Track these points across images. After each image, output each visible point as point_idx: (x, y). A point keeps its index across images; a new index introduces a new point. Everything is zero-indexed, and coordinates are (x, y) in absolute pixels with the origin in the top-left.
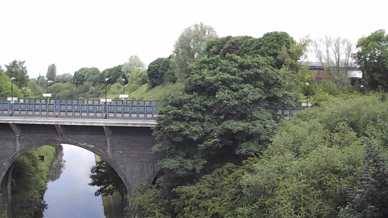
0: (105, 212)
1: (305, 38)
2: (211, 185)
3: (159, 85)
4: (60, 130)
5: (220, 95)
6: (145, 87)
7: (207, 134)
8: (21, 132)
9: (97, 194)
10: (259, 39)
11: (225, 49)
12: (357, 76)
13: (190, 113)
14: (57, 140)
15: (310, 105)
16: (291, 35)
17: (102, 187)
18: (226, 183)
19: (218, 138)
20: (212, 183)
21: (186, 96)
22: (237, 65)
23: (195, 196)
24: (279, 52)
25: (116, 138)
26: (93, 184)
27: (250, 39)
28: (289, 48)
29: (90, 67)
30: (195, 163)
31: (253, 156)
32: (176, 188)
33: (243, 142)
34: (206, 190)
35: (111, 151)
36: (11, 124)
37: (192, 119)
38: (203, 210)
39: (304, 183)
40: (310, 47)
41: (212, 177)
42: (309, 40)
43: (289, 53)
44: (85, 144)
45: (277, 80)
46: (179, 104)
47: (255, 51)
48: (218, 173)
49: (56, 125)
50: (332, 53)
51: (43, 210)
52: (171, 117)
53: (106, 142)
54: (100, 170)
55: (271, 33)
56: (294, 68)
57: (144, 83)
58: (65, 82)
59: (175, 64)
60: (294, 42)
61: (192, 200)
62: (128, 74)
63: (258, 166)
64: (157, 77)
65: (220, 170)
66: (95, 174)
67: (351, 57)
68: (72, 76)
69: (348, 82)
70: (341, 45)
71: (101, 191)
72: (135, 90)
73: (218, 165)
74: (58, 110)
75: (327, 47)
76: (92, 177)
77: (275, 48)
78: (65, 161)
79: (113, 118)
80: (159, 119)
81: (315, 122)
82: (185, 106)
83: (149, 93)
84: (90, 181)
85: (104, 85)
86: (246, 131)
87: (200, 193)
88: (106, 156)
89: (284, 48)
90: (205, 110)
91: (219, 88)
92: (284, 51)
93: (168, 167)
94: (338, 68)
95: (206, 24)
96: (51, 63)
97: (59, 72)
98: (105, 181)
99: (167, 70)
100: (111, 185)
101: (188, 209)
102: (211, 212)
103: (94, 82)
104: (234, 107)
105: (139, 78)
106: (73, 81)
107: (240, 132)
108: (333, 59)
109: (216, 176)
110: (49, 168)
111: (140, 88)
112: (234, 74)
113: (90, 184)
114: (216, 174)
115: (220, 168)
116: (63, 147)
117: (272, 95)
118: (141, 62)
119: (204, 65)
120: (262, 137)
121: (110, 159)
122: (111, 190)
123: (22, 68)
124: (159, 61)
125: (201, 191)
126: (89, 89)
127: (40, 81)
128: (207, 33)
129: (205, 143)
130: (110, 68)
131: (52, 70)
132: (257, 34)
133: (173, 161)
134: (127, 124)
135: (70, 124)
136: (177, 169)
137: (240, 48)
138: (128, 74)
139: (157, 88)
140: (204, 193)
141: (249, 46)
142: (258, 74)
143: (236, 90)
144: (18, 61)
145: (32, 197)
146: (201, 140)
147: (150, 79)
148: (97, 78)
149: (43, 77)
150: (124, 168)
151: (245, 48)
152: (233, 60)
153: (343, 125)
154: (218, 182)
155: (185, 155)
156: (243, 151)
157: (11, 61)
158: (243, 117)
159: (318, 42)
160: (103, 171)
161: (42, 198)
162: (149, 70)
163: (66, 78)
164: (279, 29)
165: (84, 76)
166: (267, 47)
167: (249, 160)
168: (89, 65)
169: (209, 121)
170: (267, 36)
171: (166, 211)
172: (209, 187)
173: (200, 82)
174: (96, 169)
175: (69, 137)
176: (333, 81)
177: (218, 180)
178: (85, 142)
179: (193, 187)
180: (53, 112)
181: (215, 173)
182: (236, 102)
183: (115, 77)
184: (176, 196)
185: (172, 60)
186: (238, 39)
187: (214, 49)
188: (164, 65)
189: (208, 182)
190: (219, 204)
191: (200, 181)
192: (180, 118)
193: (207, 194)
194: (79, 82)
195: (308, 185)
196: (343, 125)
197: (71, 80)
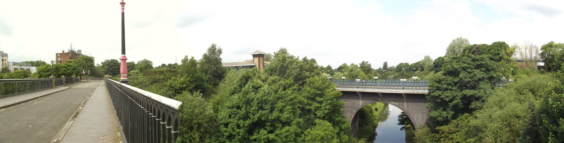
1: (514, 45)
4: (380, 96)
5: (461, 76)
6: (433, 72)
7: (454, 97)
9: (402, 129)
10: (490, 46)
11: (473, 51)
12: (541, 65)
15: (513, 80)
16: (507, 44)
17: (404, 125)
18: (463, 124)
19: (460, 99)
20: (456, 125)
21: (443, 77)
23: (446, 132)
24: (501, 52)
26: (400, 124)
28: (506, 50)
29: (404, 62)
31: (478, 109)
33: (473, 101)
34: (453, 128)
37: (446, 89)
38: (451, 140)
39: (501, 124)
40: (517, 50)
41: (457, 121)
42: (516, 46)
43: (506, 53)
45: (493, 67)
46: (439, 82)
47: (488, 52)
48: (460, 119)
50: (528, 53)
52: (435, 88)
54: (403, 117)
55: (497, 42)
56: (508, 61)
57: (432, 70)
58: (392, 71)
60: (508, 47)
62: (424, 66)
63: (478, 115)
65: (461, 117)
66: (401, 118)
67: (538, 55)
69: (536, 68)
70: (533, 49)
71: (403, 128)
72: (427, 74)
73: (460, 115)
74: (379, 85)
75: (526, 50)
76: (399, 120)
77: (499, 50)
79: (407, 89)
80: (429, 90)
81: (512, 90)
82: (442, 82)
84: (398, 122)
85: (411, 72)
87: (449, 130)
89: (503, 50)
91: (461, 72)
92: (503, 52)
93: (433, 115)
94: (531, 61)
95: (463, 38)
96: (385, 61)
97: (389, 66)
100: (409, 125)
102: (455, 141)
104: (469, 82)
105: (429, 68)
107: (470, 96)
108: (529, 56)
109: (459, 120)
110: (380, 114)
111: (430, 73)
112: (469, 64)
113: (398, 124)
114: (459, 119)
115: (461, 116)
117: (491, 75)
119: (453, 60)
120: (484, 99)
121: (406, 111)
122: (409, 128)
124: (439, 58)
125: (450, 129)
127: (379, 71)
128: (464, 43)
129: (453, 102)
130: (414, 63)
131: (385, 65)
132: (490, 43)
134: (385, 91)
135: (391, 92)
137: (480, 50)
138: (424, 66)
140: (451, 131)
142: (482, 64)
143: (470, 73)
144: (365, 61)
146: (451, 101)
148: (408, 68)
149: (381, 68)
153: (526, 91)
154: (460, 124)
155: (442, 109)
157: (362, 61)
158: (474, 88)
159: (521, 47)
161: (374, 130)
162: (434, 63)
163: (392, 69)
164: (501, 40)
166: (494, 50)
169: (455, 90)
170: (494, 44)
171: (433, 140)
172: (455, 127)
173: (450, 69)
174: (400, 116)
175: (385, 99)
176: (529, 67)
177: (460, 123)
178: (393, 102)
181: (458, 119)
182: (188, 78)
188: (442, 60)
190: (460, 137)
191: (450, 124)
192: (438, 89)
193: (453, 131)
194: (399, 71)
195: (502, 125)
196: (526, 91)
197: (395, 69)
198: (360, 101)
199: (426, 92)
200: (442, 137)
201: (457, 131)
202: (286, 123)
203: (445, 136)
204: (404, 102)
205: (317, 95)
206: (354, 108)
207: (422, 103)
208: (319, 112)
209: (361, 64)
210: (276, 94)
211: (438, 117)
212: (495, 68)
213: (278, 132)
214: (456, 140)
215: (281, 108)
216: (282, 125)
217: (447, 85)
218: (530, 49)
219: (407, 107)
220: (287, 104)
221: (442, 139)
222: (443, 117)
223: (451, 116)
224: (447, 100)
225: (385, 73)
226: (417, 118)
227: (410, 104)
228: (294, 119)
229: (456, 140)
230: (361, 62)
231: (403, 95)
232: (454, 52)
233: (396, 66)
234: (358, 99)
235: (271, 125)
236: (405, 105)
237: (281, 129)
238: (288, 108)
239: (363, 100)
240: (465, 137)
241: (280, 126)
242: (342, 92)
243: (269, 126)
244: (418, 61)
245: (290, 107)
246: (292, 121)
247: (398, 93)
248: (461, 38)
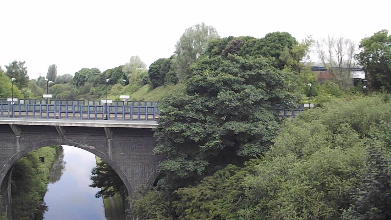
0: (105, 214)
1: (308, 39)
2: (212, 187)
3: (160, 86)
4: (61, 131)
5: (221, 96)
6: (146, 88)
7: (209, 135)
8: (21, 133)
9: (97, 196)
10: (261, 39)
11: (227, 50)
12: (359, 77)
13: (192, 114)
14: (57, 141)
15: (312, 106)
16: (293, 36)
17: (103, 188)
18: (227, 184)
19: (220, 139)
20: (214, 185)
21: (188, 97)
23: (196, 198)
24: (281, 52)
25: (117, 139)
26: (94, 186)
27: (252, 40)
28: (291, 48)
29: (90, 67)
32: (177, 190)
33: (245, 143)
34: (208, 192)
35: (112, 152)
36: (11, 125)
37: (194, 120)
38: (204, 212)
39: (306, 185)
40: (313, 48)
41: (214, 178)
42: (311, 40)
43: (291, 53)
44: (86, 145)
45: (280, 80)
46: (180, 105)
47: (257, 51)
48: (220, 175)
49: (56, 126)
50: (334, 54)
51: (44, 212)
52: (173, 118)
53: (107, 143)
54: (101, 172)
55: (273, 33)
56: (296, 68)
57: (145, 84)
58: (65, 83)
59: (176, 65)
60: (296, 43)
61: (193, 201)
62: (129, 75)
63: (260, 168)
64: (158, 78)
65: (221, 172)
66: (96, 175)
67: (354, 57)
68: (72, 76)
69: (351, 82)
70: (344, 46)
71: (101, 192)
72: (136, 91)
73: (220, 167)
74: (58, 111)
75: (330, 48)
76: (93, 178)
77: (277, 48)
78: (65, 163)
79: (114, 119)
80: (160, 120)
81: (317, 123)
82: (187, 107)
83: (150, 94)
84: (91, 182)
85: (105, 85)
86: (248, 132)
87: (201, 195)
88: (106, 157)
89: (286, 48)
90: (207, 111)
91: (221, 89)
92: (286, 52)
93: (169, 168)
95: (207, 24)
96: (51, 64)
97: (60, 73)
99: (168, 71)
100: (112, 187)
101: (190, 211)
102: (212, 214)
103: (94, 83)
105: (140, 79)
106: (73, 82)
107: (242, 133)
108: (336, 60)
109: (218, 177)
111: (141, 89)
112: (236, 75)
113: (91, 186)
114: (218, 176)
115: (221, 169)
116: (64, 148)
117: (274, 96)
118: (142, 63)
119: (206, 65)
120: (265, 139)
121: (111, 160)
122: (112, 192)
123: (22, 68)
124: (160, 61)
125: (203, 193)
126: (89, 90)
127: (40, 82)
128: (209, 33)
129: (207, 144)
130: (111, 68)
131: (52, 71)
132: (259, 34)
133: (175, 162)
134: (128, 125)
135: (70, 125)
136: (178, 171)
138: (129, 75)
139: (158, 89)
140: (206, 195)
141: (251, 46)
142: (260, 75)
143: (238, 91)
144: (18, 62)
145: (32, 198)
146: (202, 142)
147: (151, 80)
148: (98, 79)
149: (44, 78)
150: (125, 169)
152: (235, 61)
153: (346, 126)
154: (219, 184)
155: (186, 156)
156: (245, 152)
157: (11, 61)
158: (244, 118)
159: (320, 43)
160: (104, 172)
161: (42, 200)
162: (150, 70)
163: (66, 78)
164: (281, 29)
165: (84, 77)
166: (269, 48)
167: (251, 161)
168: (90, 66)
169: (210, 122)
170: (269, 36)
171: (167, 213)
172: (211, 189)
173: (201, 83)
174: (96, 171)
175: (70, 139)
176: (336, 82)
177: (219, 182)
178: (86, 143)
179: (194, 189)
180: (53, 113)
181: (216, 174)
183: (116, 78)
184: (178, 198)
185: (174, 61)
186: (240, 40)
187: (216, 49)
188: (165, 65)
189: (210, 183)
191: (201, 183)
192: (181, 119)
193: (209, 196)
194: (80, 83)
195: (311, 187)
196: (346, 126)
197: (72, 80)
203: (193, 205)
206: (5, 158)
212: (283, 82)
218: (338, 45)
221: (188, 211)
229: (214, 213)
240: (233, 206)
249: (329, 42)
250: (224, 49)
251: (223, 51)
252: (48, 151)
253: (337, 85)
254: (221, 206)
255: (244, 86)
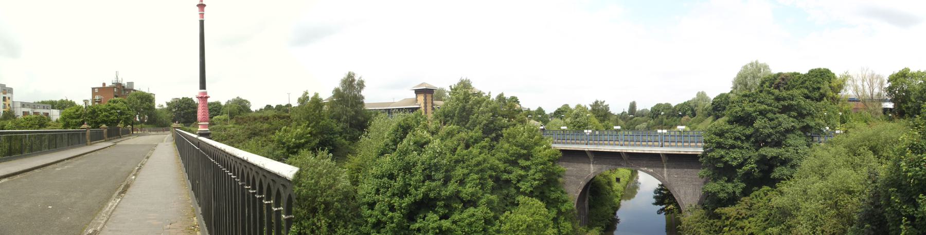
1: (844, 74)
4: (625, 157)
5: (757, 124)
6: (710, 119)
7: (746, 160)
9: (659, 212)
10: (804, 75)
11: (776, 84)
12: (888, 107)
15: (842, 132)
16: (832, 72)
17: (664, 206)
18: (761, 204)
19: (755, 163)
20: (749, 205)
21: (728, 127)
22: (773, 97)
23: (732, 217)
24: (822, 86)
26: (656, 204)
28: (830, 83)
29: (664, 103)
30: (735, 186)
33: (777, 167)
34: (744, 211)
37: (733, 147)
38: (740, 230)
39: (822, 204)
41: (750, 199)
42: (848, 75)
43: (830, 87)
45: (810, 110)
46: (721, 134)
47: (801, 85)
48: (756, 196)
50: (867, 87)
52: (714, 145)
54: (662, 191)
55: (815, 69)
56: (834, 100)
57: (709, 116)
58: (643, 116)
60: (835, 77)
62: (696, 108)
63: (785, 189)
65: (757, 193)
66: (658, 195)
67: (883, 90)
69: (881, 112)
70: (875, 80)
71: (662, 210)
72: (702, 122)
73: (756, 188)
74: (622, 140)
75: (863, 82)
76: (655, 197)
77: (819, 82)
79: (668, 146)
80: (705, 148)
81: (841, 148)
82: (726, 135)
84: (654, 201)
85: (675, 118)
87: (737, 214)
89: (826, 83)
91: (757, 118)
92: (825, 86)
93: (710, 190)
95: (761, 62)
96: (632, 101)
97: (639, 108)
98: (667, 201)
100: (671, 205)
102: (747, 232)
105: (705, 112)
107: (772, 158)
108: (868, 92)
109: (753, 198)
111: (706, 120)
112: (771, 106)
113: (654, 204)
114: (754, 196)
115: (757, 190)
117: (806, 124)
119: (745, 98)
120: (794, 162)
121: (666, 182)
122: (672, 210)
124: (722, 96)
125: (739, 212)
127: (623, 116)
128: (762, 70)
129: (744, 168)
130: (680, 103)
131: (633, 106)
132: (804, 71)
134: (633, 150)
135: (642, 152)
138: (696, 108)
140: (741, 215)
142: (792, 105)
143: (771, 120)
144: (599, 101)
146: (741, 165)
148: (670, 112)
149: (626, 112)
151: (793, 83)
153: (864, 149)
154: (755, 204)
155: (726, 179)
157: (594, 101)
158: (778, 144)
159: (855, 78)
161: (615, 214)
162: (713, 104)
163: (644, 113)
164: (822, 66)
166: (811, 82)
169: (747, 148)
170: (812, 72)
171: (711, 230)
172: (747, 209)
173: (740, 113)
174: (657, 191)
175: (632, 163)
176: (868, 111)
177: (755, 202)
178: (646, 167)
181: (752, 195)
188: (726, 99)
191: (738, 203)
192: (720, 146)
193: (744, 215)
194: (655, 116)
195: (825, 206)
196: (864, 149)
197: (649, 114)
198: (591, 165)
199: (700, 151)
200: (726, 226)
201: (751, 216)
202: (469, 201)
204: (663, 167)
205: (520, 156)
207: (693, 170)
208: (524, 185)
209: (593, 105)
210: (454, 155)
211: (719, 192)
212: (813, 111)
213: (456, 216)
214: (749, 230)
215: (461, 177)
216: (464, 206)
217: (734, 140)
219: (669, 175)
220: (471, 171)
222: (727, 193)
223: (741, 190)
224: (734, 164)
225: (632, 120)
226: (685, 193)
227: (673, 170)
228: (483, 195)
230: (592, 102)
231: (661, 155)
232: (746, 85)
233: (649, 109)
234: (587, 163)
235: (445, 205)
236: (665, 172)
237: (462, 212)
238: (472, 178)
239: (596, 164)
240: (764, 224)
241: (460, 207)
242: (561, 150)
243: (441, 207)
244: (686, 101)
245: (475, 176)
246: (479, 198)
247: (653, 152)
248: (757, 62)
249: (862, 77)
250: (773, 84)
251: (773, 85)
252: (623, 172)
253: (869, 114)
254: (755, 225)
255: (778, 115)
